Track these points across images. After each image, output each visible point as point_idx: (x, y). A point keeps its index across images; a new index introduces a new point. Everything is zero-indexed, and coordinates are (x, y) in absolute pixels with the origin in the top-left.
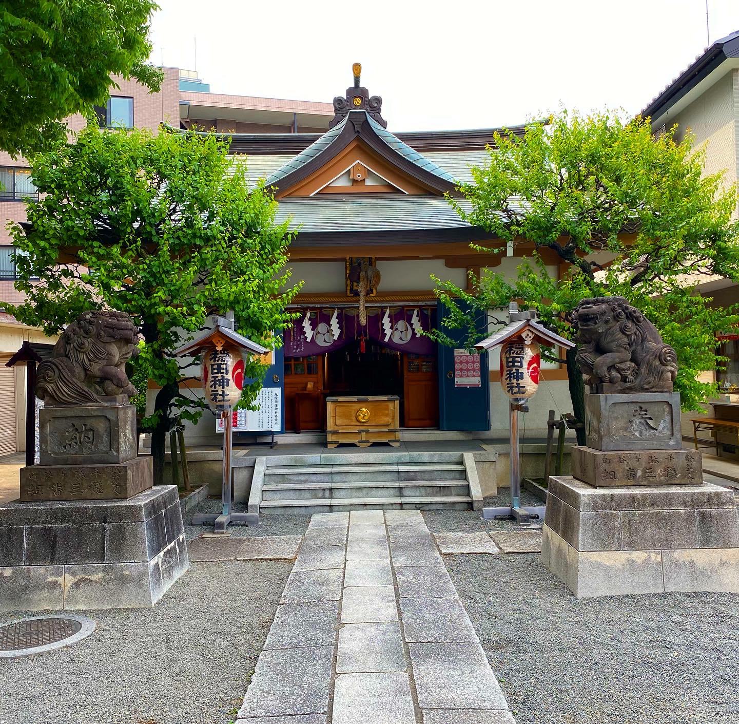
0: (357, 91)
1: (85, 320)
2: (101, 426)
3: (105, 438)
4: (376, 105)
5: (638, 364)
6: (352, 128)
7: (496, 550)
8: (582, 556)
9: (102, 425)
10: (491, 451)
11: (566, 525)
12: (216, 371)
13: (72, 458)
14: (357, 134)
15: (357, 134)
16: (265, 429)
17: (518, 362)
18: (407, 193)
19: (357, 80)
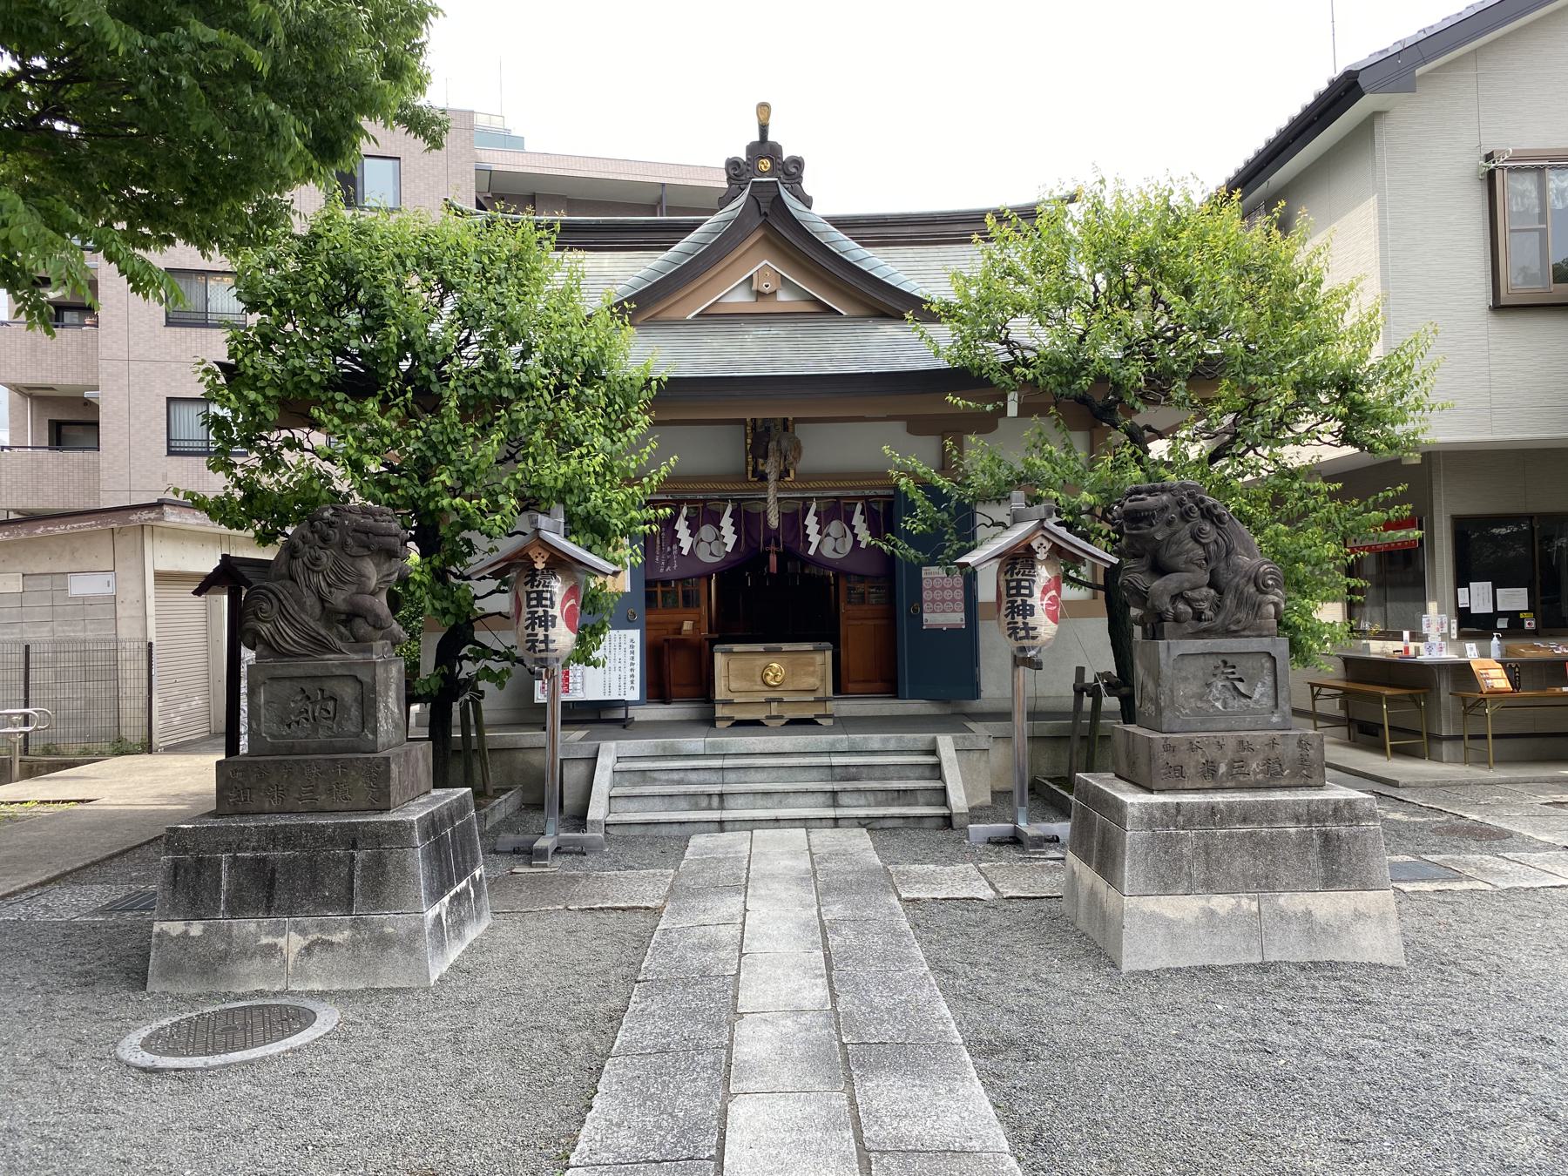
0: (763, 148)
1: (322, 519)
2: (347, 692)
3: (354, 712)
5: (1220, 592)
7: (988, 894)
8: (1129, 903)
10: (981, 732)
11: (1105, 858)
16: (614, 696)
19: (764, 129)
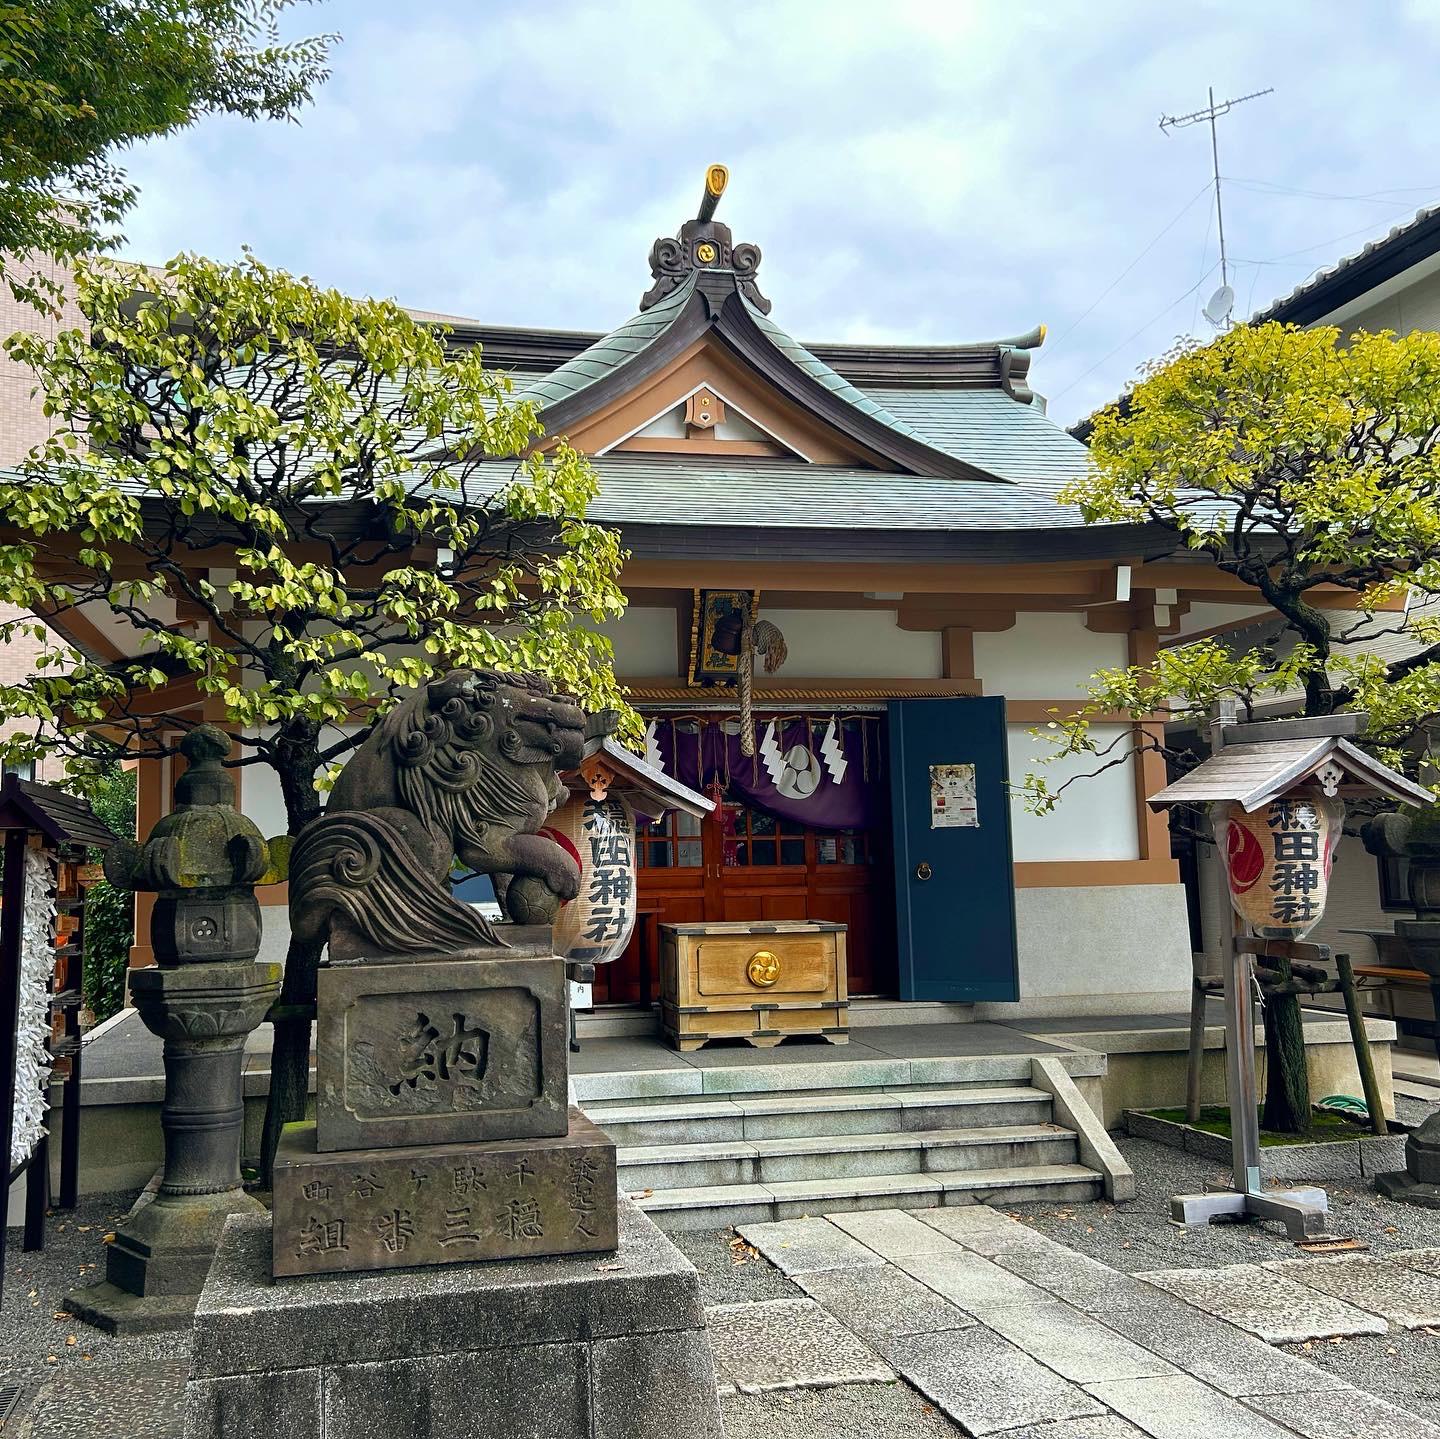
1: (462, 694)
2: (508, 1021)
3: (522, 1058)
4: (747, 263)
6: (701, 308)
9: (512, 1017)
12: (605, 857)
13: (419, 1124)
14: (711, 323)
15: (711, 323)
17: (1307, 846)
18: (810, 461)
19: (710, 202)
